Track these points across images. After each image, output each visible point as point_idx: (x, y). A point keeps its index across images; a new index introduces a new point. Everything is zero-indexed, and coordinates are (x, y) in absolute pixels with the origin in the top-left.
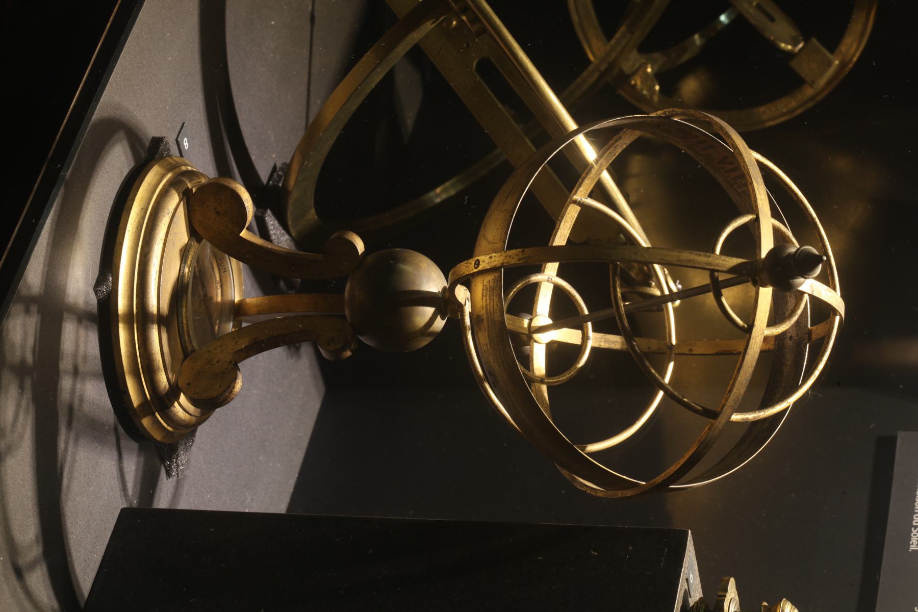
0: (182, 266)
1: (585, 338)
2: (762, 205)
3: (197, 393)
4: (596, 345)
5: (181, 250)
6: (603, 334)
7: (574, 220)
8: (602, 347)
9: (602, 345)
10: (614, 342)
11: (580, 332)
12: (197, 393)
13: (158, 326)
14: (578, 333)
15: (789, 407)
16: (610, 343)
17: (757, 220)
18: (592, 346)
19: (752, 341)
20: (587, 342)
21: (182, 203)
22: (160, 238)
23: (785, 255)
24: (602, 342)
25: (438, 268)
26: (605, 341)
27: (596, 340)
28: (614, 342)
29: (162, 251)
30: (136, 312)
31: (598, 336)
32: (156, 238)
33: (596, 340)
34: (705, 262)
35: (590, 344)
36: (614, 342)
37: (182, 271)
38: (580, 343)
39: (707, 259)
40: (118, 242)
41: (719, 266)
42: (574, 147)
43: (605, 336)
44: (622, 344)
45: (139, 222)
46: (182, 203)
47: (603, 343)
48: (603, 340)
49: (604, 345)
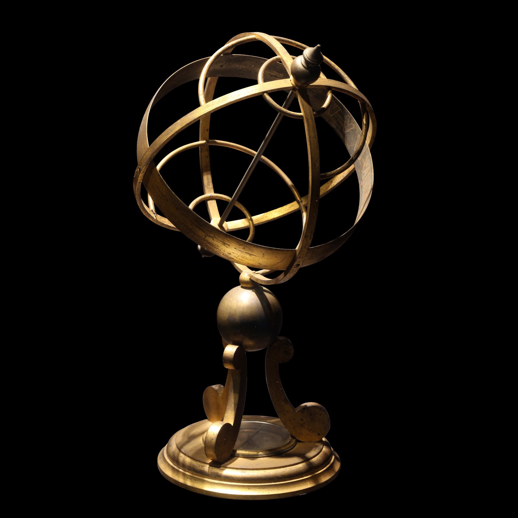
0: (260, 456)
1: (211, 198)
2: (256, 90)
3: (326, 428)
4: (213, 190)
5: (253, 460)
8: (212, 186)
9: (212, 187)
10: (207, 180)
12: (326, 428)
13: (310, 460)
14: (209, 202)
15: (282, 63)
16: (209, 182)
18: (214, 192)
20: (214, 197)
21: (228, 466)
22: (264, 472)
23: (307, 71)
24: (210, 187)
25: (225, 295)
26: (209, 185)
27: (209, 192)
28: (207, 180)
29: (281, 468)
30: (310, 475)
31: (207, 190)
32: (266, 475)
33: (209, 192)
34: (311, 121)
36: (208, 180)
37: (264, 456)
38: (215, 201)
39: (310, 120)
40: (277, 498)
41: (311, 111)
43: (206, 186)
44: (208, 174)
45: (259, 488)
46: (228, 466)
47: (210, 186)
48: (208, 187)
49: (211, 186)
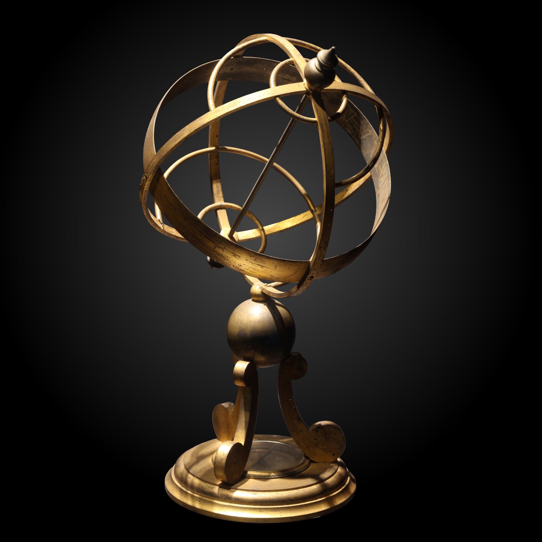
0: (273, 477)
1: (221, 207)
2: (268, 94)
4: (222, 199)
5: (264, 481)
6: (215, 196)
7: (169, 227)
8: (222, 195)
9: (222, 196)
11: (218, 211)
12: (341, 448)
13: (324, 481)
16: (218, 190)
17: (281, 97)
18: (223, 201)
19: (352, 90)
21: (238, 488)
22: (276, 494)
23: (322, 74)
24: (219, 196)
26: (219, 194)
27: (219, 201)
28: (217, 187)
29: (294, 490)
30: (324, 497)
31: (217, 199)
32: (278, 497)
33: (219, 201)
34: (326, 126)
35: (224, 203)
36: (218, 188)
37: (276, 477)
39: (324, 125)
40: (290, 521)
42: (254, 227)
43: (215, 195)
45: (271, 511)
46: (238, 488)
47: (220, 195)
48: (218, 195)
49: (221, 194)
